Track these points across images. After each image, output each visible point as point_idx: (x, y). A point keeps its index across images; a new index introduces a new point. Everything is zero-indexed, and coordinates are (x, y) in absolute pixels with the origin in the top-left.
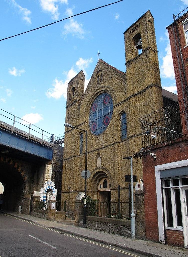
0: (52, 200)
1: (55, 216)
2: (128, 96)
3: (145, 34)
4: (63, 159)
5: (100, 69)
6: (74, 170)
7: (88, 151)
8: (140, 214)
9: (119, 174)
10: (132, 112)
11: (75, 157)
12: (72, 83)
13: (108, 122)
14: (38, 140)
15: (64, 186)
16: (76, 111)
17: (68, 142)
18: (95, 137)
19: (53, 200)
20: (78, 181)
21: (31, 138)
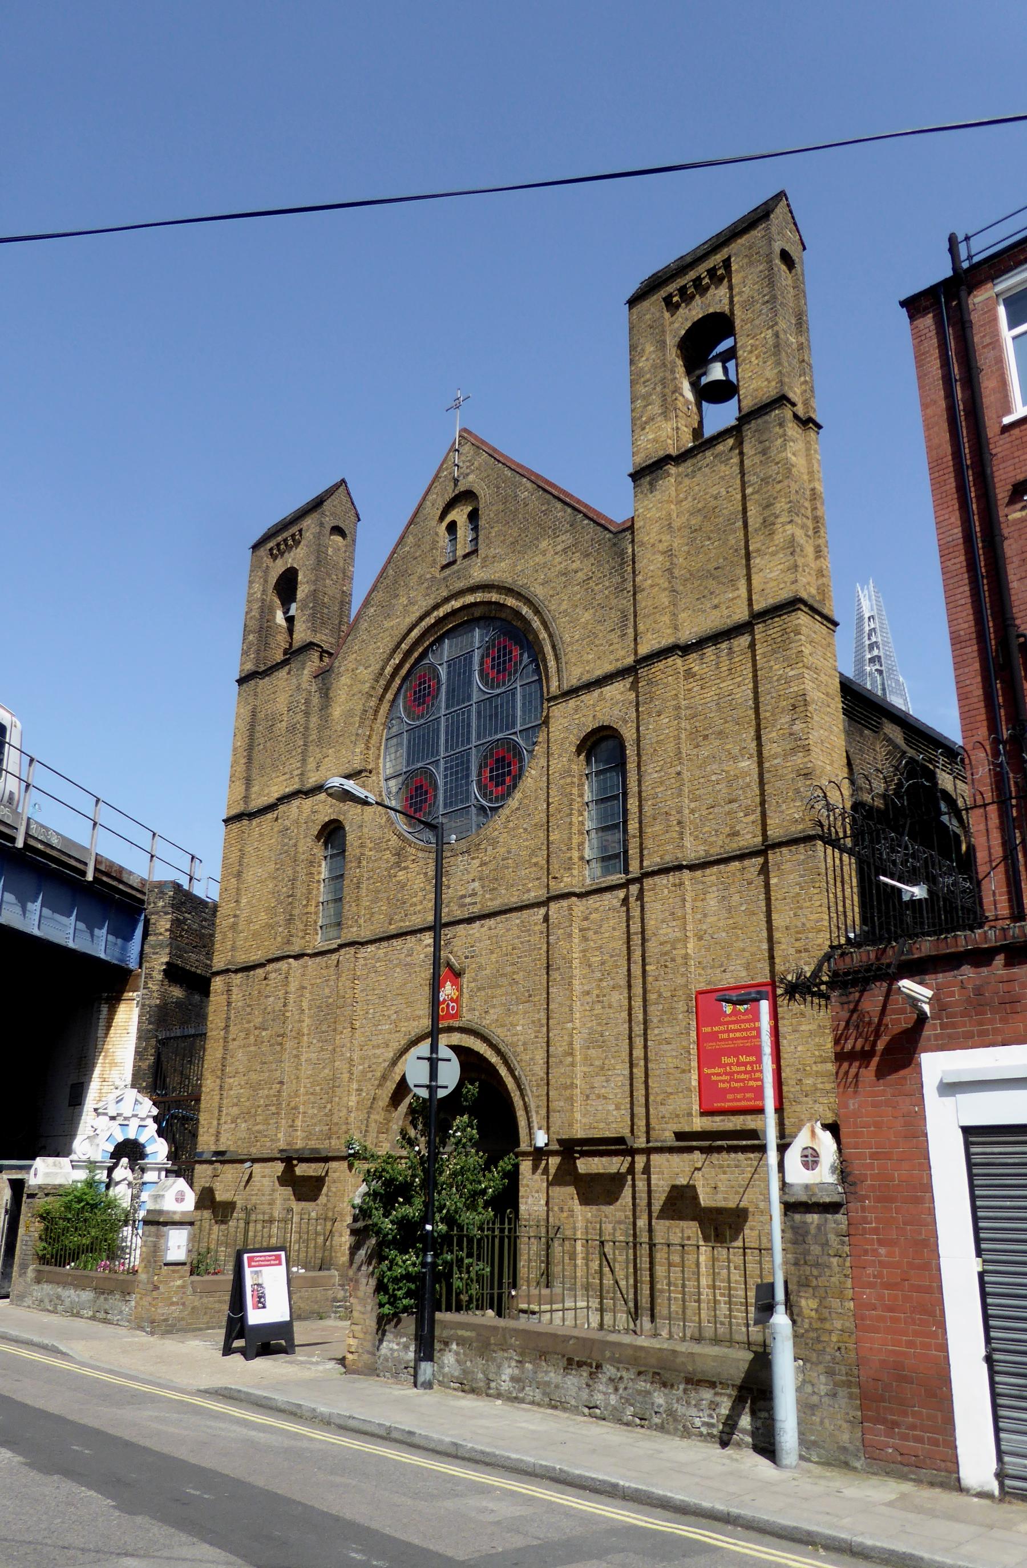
0: (168, 1212)
1: (183, 1304)
2: (644, 650)
3: (757, 322)
4: (214, 969)
5: (462, 487)
6: (282, 1035)
7: (428, 939)
8: (822, 1320)
9: (573, 1064)
10: (662, 737)
11: (291, 960)
12: (278, 545)
13: (507, 778)
14: (70, 856)
15: (215, 1122)
16: (307, 702)
17: (249, 876)
18: (420, 854)
19: (175, 1213)
20: (307, 1093)
21: (32, 842)
